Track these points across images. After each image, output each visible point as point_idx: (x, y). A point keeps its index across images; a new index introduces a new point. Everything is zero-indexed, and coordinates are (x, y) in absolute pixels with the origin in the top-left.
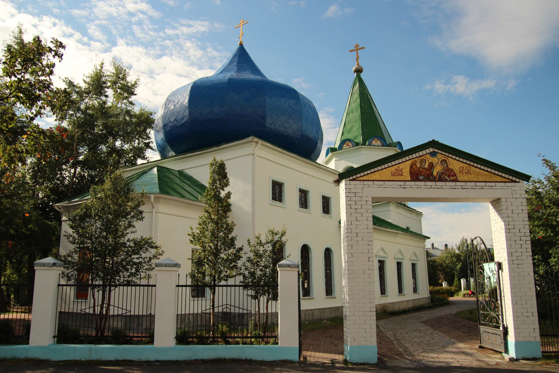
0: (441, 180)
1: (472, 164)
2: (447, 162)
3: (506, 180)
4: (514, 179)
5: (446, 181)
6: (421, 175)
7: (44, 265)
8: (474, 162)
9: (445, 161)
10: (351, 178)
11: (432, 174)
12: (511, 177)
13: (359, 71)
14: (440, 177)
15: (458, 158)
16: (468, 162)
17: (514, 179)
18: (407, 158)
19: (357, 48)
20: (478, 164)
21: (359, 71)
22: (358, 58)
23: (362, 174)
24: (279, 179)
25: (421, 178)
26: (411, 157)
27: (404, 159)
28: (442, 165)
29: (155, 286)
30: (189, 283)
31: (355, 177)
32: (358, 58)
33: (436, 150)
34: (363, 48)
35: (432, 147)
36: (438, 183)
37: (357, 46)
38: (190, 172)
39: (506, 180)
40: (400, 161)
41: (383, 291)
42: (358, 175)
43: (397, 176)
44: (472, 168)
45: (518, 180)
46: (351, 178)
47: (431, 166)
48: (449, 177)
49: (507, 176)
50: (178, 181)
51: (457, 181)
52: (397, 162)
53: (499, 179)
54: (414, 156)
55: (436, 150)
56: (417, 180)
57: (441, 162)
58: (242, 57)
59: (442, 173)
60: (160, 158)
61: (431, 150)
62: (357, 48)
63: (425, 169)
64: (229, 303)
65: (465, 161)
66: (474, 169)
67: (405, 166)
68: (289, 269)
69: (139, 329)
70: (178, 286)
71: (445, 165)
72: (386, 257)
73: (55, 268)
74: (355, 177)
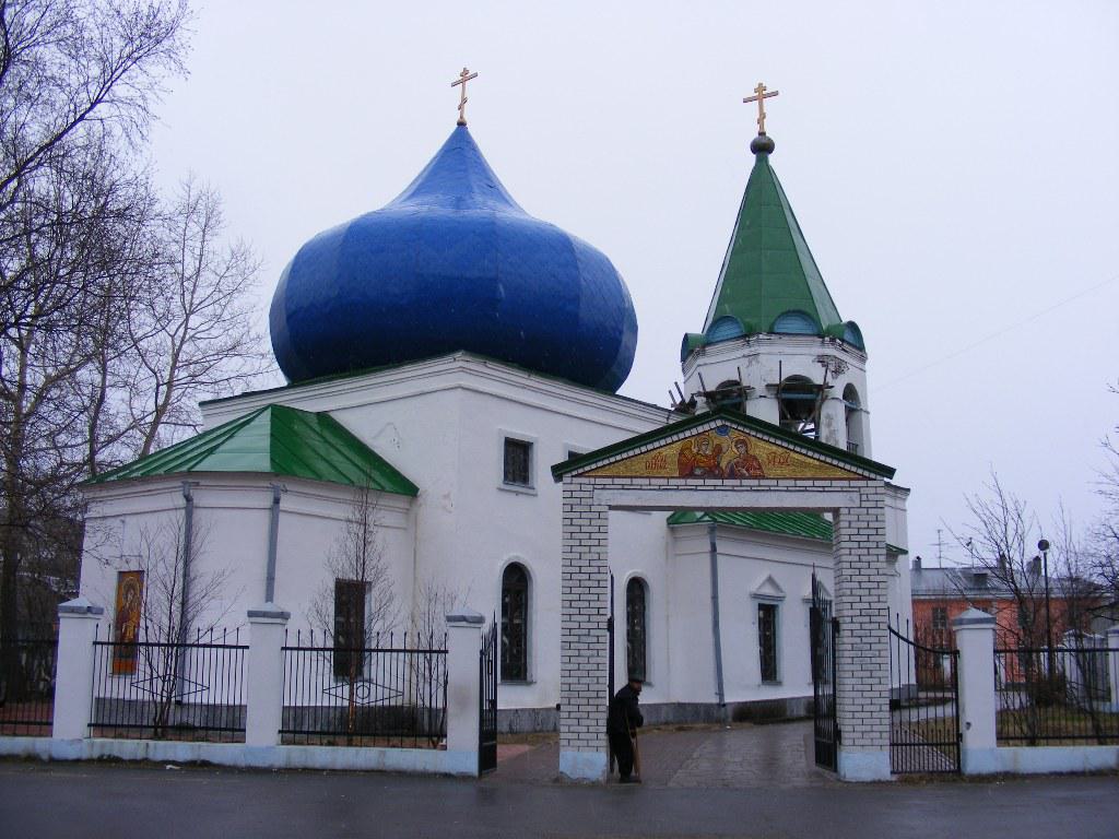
0: (732, 475)
1: (791, 447)
2: (746, 445)
3: (852, 476)
4: (866, 474)
5: (742, 477)
6: (699, 467)
7: (73, 610)
8: (796, 445)
9: (743, 442)
10: (574, 473)
11: (718, 466)
12: (860, 471)
13: (762, 148)
14: (732, 470)
15: (766, 438)
16: (785, 444)
17: (866, 474)
18: (675, 438)
19: (466, 76)
20: (802, 447)
21: (762, 148)
22: (762, 116)
23: (594, 466)
24: (520, 433)
25: (698, 472)
26: (681, 436)
27: (669, 440)
28: (737, 448)
29: (247, 647)
30: (330, 644)
31: (580, 471)
32: (762, 116)
33: (728, 424)
34: (775, 94)
35: (722, 418)
36: (726, 482)
37: (761, 88)
38: (343, 419)
39: (852, 476)
40: (663, 442)
41: (769, 672)
42: (587, 468)
43: (654, 469)
44: (792, 454)
45: (873, 476)
46: (574, 473)
47: (718, 450)
48: (747, 470)
49: (854, 469)
50: (316, 442)
51: (764, 478)
52: (656, 444)
53: (839, 474)
54: (688, 434)
55: (728, 424)
56: (691, 475)
57: (737, 442)
58: (459, 157)
59: (737, 464)
60: (284, 383)
61: (719, 423)
62: (761, 94)
63: (706, 456)
64: (394, 687)
65: (779, 442)
66: (796, 456)
67: (670, 449)
68: (464, 624)
69: (227, 723)
70: (95, 643)
71: (743, 450)
72: (781, 599)
73: (89, 615)
74: (580, 471)
